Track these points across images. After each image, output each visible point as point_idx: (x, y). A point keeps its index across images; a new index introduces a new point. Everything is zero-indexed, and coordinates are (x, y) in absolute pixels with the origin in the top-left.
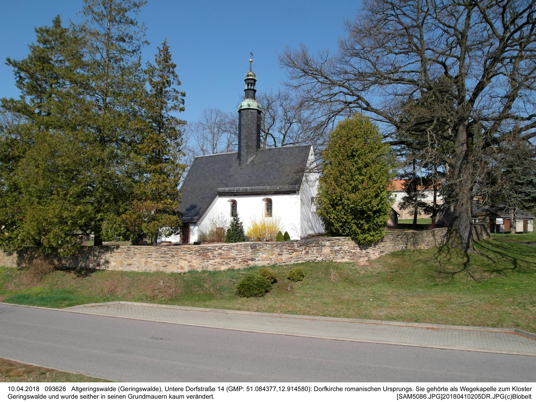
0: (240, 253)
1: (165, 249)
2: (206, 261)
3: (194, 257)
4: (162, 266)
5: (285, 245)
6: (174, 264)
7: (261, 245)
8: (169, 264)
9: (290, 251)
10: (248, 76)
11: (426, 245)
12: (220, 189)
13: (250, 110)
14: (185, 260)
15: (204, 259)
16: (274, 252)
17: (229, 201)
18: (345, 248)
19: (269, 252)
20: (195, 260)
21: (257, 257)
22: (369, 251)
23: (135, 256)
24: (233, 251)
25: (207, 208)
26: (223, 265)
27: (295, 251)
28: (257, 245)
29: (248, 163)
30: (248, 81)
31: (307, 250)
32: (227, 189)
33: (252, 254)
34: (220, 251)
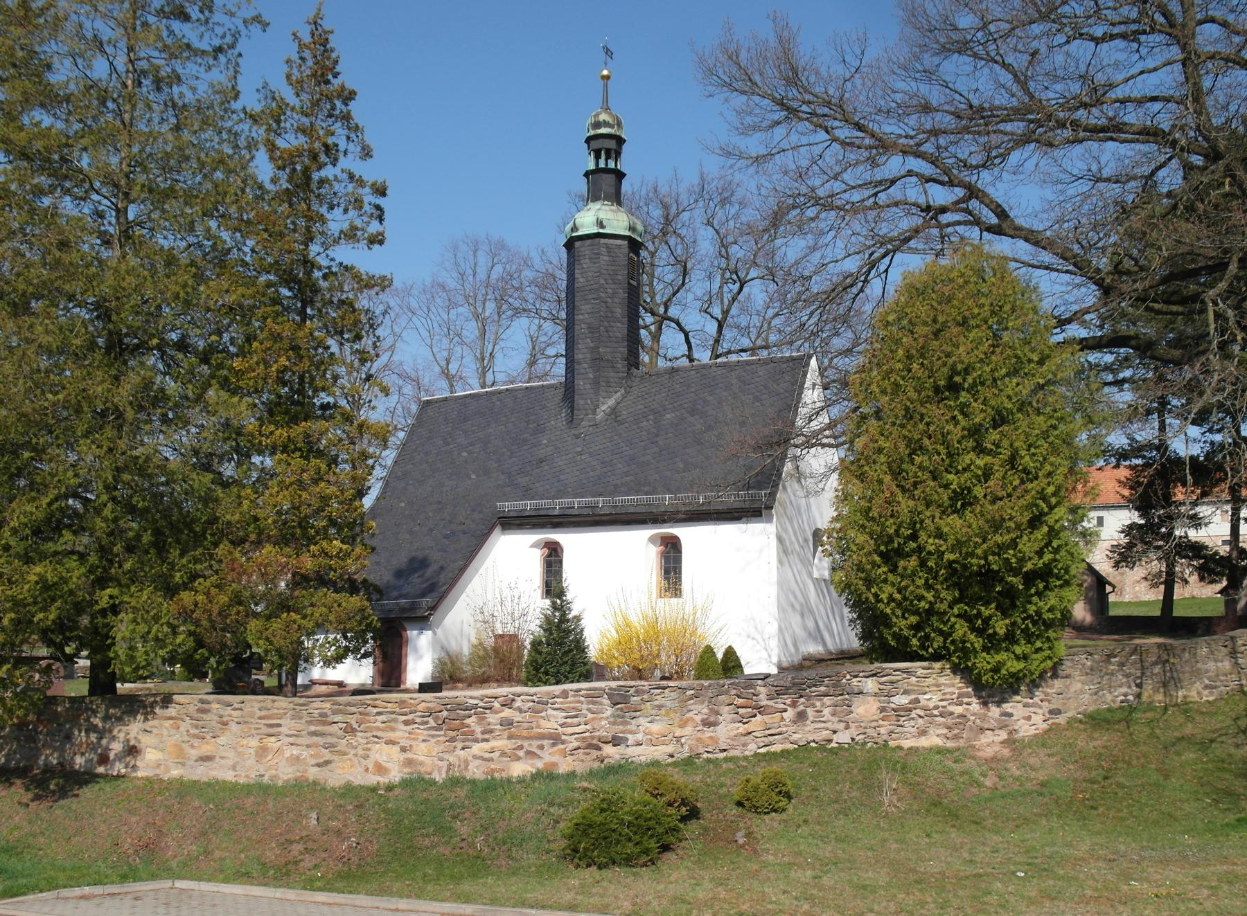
2: (460, 745)
3: (422, 733)
4: (314, 761)
5: (726, 693)
6: (356, 755)
8: (336, 758)
9: (741, 711)
10: (597, 125)
11: (1206, 687)
12: (507, 506)
13: (603, 241)
14: (391, 742)
15: (452, 740)
17: (534, 545)
18: (931, 699)
19: (672, 715)
20: (423, 745)
22: (1010, 710)
24: (550, 712)
25: (463, 569)
26: (519, 759)
27: (762, 710)
28: (632, 691)
29: (600, 416)
31: (802, 707)
32: (529, 505)
33: (614, 723)
34: (507, 713)
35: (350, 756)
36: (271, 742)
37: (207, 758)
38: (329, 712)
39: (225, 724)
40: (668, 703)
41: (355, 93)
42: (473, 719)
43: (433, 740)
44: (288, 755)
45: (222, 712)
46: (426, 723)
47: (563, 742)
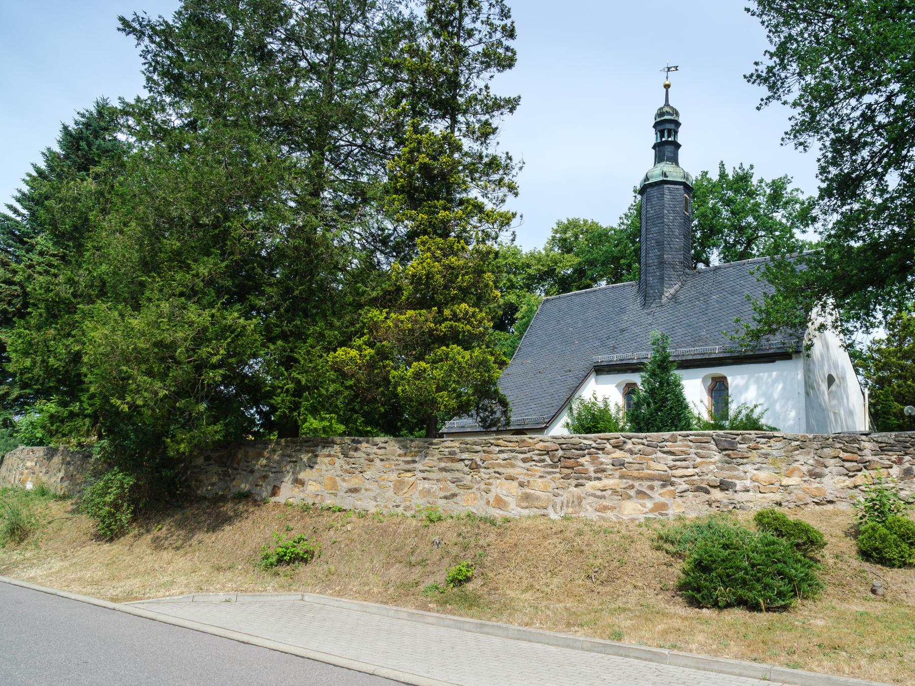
0: (684, 464)
1: (453, 444)
2: (574, 482)
3: (539, 469)
4: (442, 494)
5: (831, 446)
6: (479, 489)
7: (751, 440)
8: (461, 491)
9: (847, 464)
12: (603, 358)
14: (511, 478)
15: (566, 477)
16: (796, 465)
19: (779, 464)
20: (540, 480)
21: (738, 478)
23: (369, 467)
24: (660, 454)
26: (630, 497)
27: (867, 465)
28: (739, 438)
30: (660, 128)
31: (907, 465)
32: (615, 358)
33: (722, 469)
34: (618, 454)
35: (474, 490)
36: (408, 477)
37: (355, 490)
38: (458, 451)
39: (371, 461)
40: (775, 452)
41: (510, 66)
42: (587, 458)
43: (549, 477)
44: (420, 489)
45: (369, 450)
46: (543, 461)
47: (672, 484)
